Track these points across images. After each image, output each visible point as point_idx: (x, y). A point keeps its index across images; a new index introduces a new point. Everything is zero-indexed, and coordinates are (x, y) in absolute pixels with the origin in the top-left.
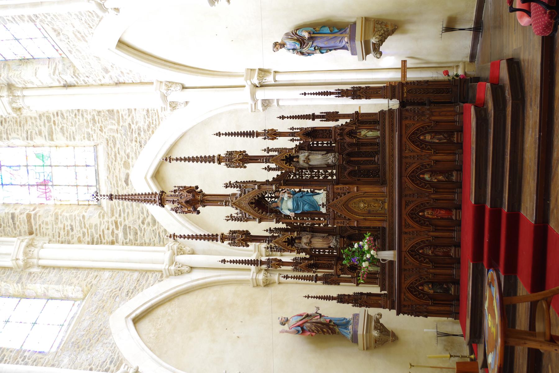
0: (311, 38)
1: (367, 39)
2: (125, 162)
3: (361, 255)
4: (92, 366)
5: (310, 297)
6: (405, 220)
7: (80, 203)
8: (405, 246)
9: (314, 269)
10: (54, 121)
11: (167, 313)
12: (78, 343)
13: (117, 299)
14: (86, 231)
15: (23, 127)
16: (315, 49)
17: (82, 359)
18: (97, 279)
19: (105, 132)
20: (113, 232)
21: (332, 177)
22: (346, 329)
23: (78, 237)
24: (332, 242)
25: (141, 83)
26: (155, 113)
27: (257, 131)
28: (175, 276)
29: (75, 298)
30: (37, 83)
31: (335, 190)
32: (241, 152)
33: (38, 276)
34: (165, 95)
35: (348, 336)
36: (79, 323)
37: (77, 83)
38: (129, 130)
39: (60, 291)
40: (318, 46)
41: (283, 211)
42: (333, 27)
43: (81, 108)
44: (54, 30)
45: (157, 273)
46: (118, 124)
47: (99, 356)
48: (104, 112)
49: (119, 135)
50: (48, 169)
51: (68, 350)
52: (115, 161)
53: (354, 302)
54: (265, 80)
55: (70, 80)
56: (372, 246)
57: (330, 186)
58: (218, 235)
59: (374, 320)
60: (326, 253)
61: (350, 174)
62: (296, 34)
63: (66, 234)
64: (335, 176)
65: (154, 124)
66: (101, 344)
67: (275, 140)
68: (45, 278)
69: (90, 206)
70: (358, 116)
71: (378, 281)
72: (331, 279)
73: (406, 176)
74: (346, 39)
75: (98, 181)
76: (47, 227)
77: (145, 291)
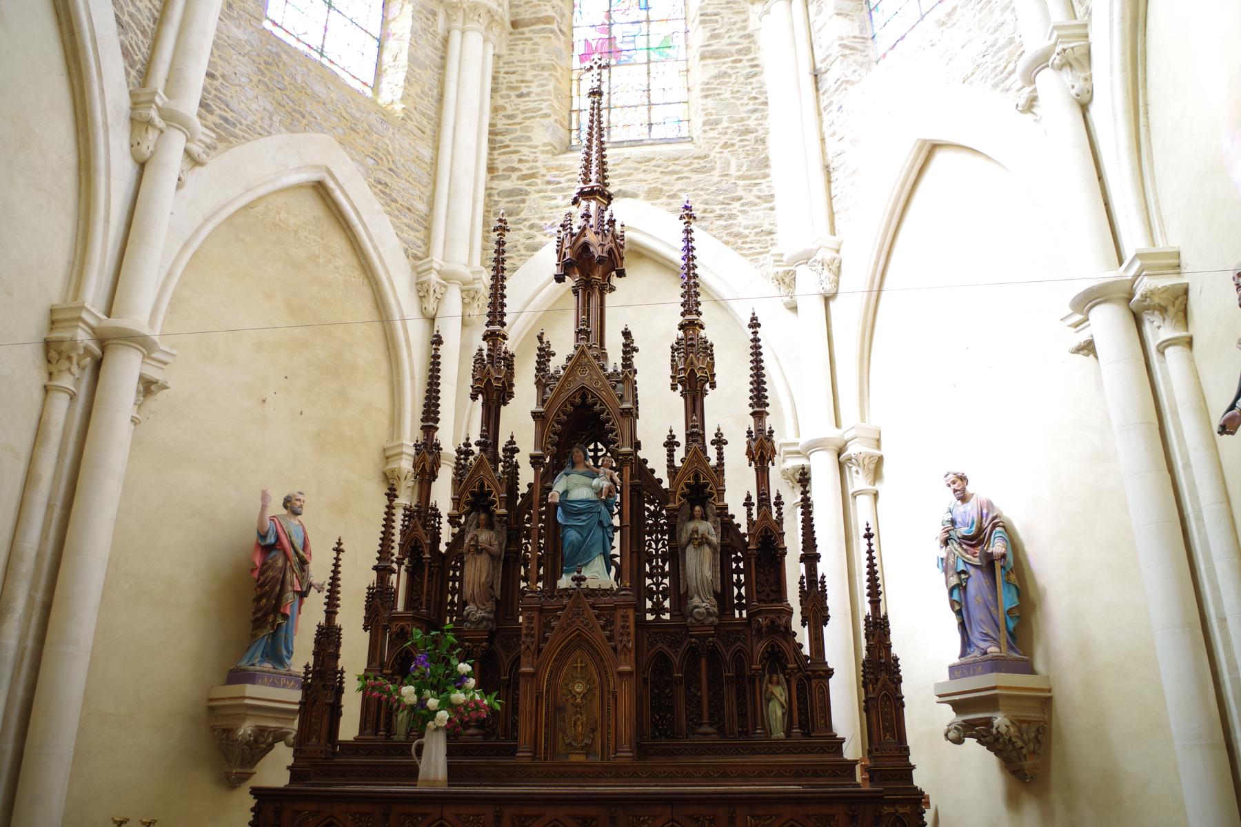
0: (989, 564)
1: (1001, 702)
2: (661, 190)
3: (439, 682)
4: (221, 80)
5: (338, 554)
6: (539, 817)
7: (574, 115)
8: (458, 816)
9: (410, 562)
10: (741, 61)
11: (333, 256)
12: (277, 64)
13: (371, 162)
14: (517, 120)
15: (726, 8)
16: (959, 573)
17: (238, 63)
18: (416, 132)
19: (722, 152)
20: (514, 169)
21: (651, 611)
22: (262, 656)
23: (505, 105)
24: (478, 608)
25: (832, 214)
26: (766, 247)
27: (768, 414)
28: (417, 284)
29: (378, 88)
30: (817, 22)
31: (620, 612)
32: (713, 375)
33: (429, 26)
34: (809, 259)
35: (246, 660)
36: (322, 78)
37: (824, 93)
38: (728, 198)
39: (395, 60)
40: (970, 581)
41: (562, 477)
42: (1018, 617)
43: (771, 109)
44: (951, 12)
45: (423, 249)
46: (739, 178)
47: (243, 98)
48: (763, 149)
49: (716, 179)
50: (641, 57)
51: (261, 41)
52: (662, 172)
53: (318, 668)
54: (857, 472)
55: (828, 81)
56: (462, 714)
57: (631, 598)
58: (502, 327)
59: (282, 728)
60: (450, 597)
61: (662, 657)
62: (995, 526)
63: (511, 85)
64: (654, 617)
65: (744, 246)
66: (268, 107)
67: (746, 459)
68: (424, 37)
69: (568, 132)
70: (820, 677)
71: (371, 735)
72: (380, 607)
73: (673, 820)
74: (993, 650)
75: (618, 145)
76: (526, 52)
77: (387, 217)
